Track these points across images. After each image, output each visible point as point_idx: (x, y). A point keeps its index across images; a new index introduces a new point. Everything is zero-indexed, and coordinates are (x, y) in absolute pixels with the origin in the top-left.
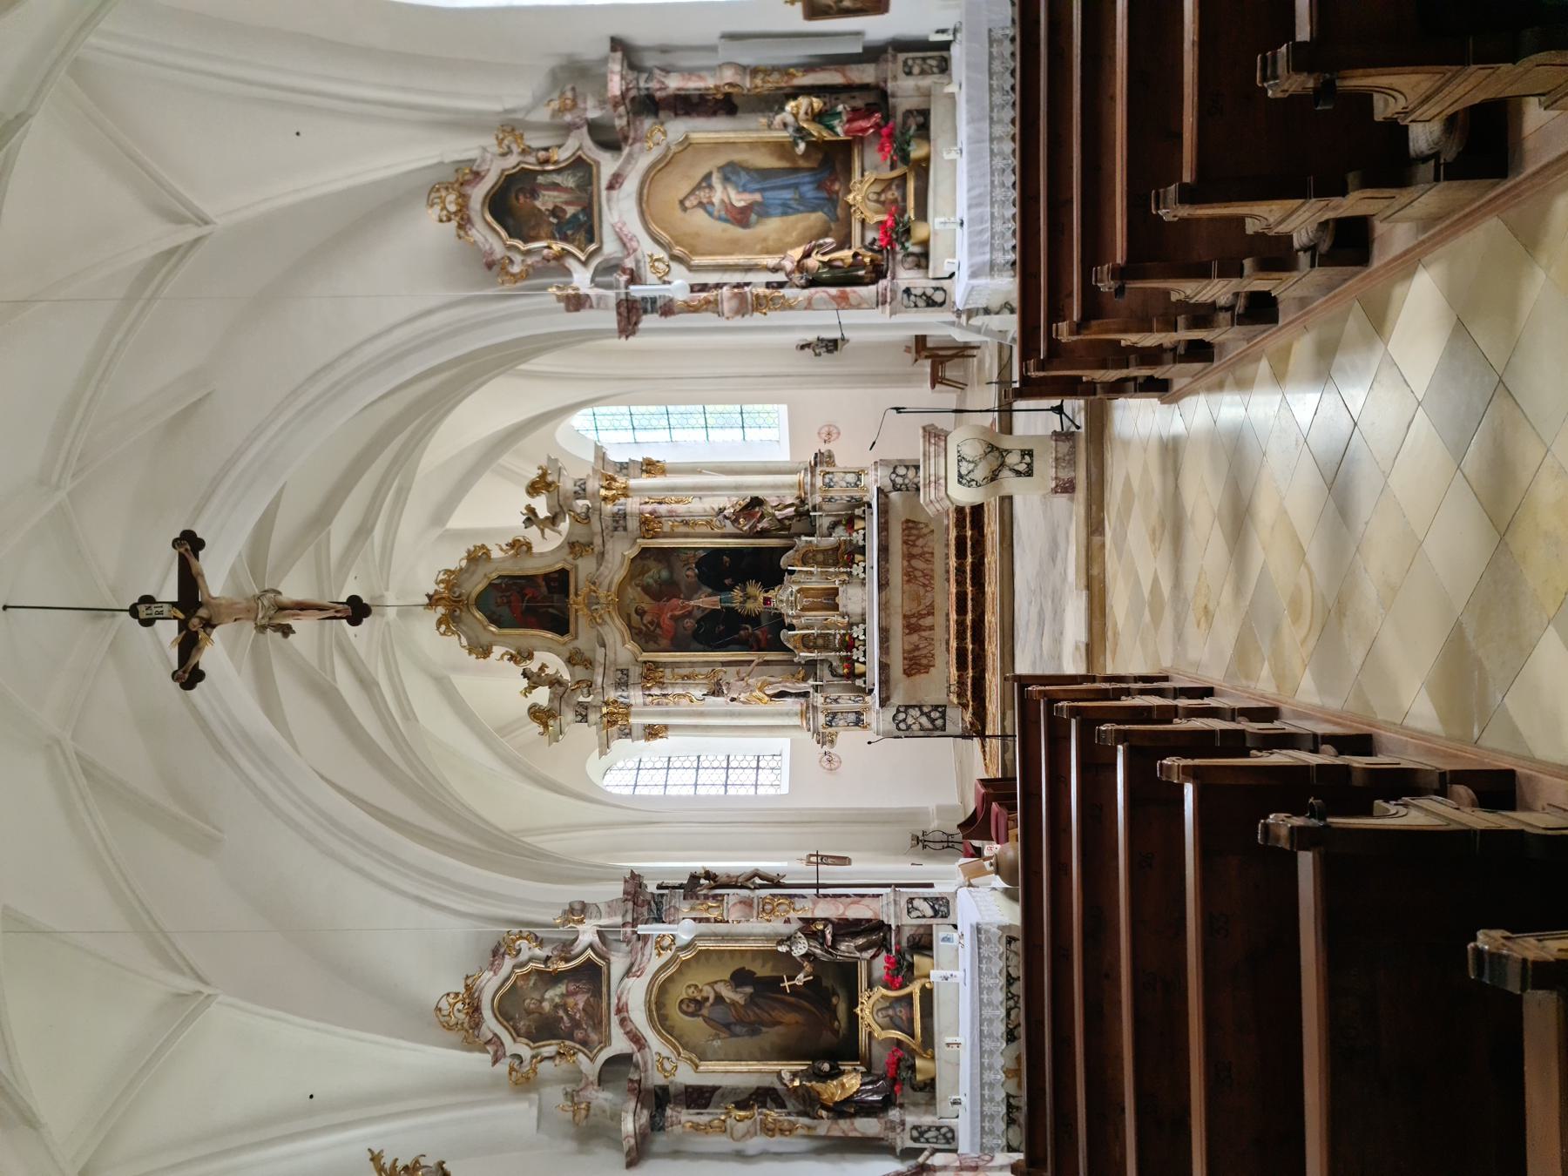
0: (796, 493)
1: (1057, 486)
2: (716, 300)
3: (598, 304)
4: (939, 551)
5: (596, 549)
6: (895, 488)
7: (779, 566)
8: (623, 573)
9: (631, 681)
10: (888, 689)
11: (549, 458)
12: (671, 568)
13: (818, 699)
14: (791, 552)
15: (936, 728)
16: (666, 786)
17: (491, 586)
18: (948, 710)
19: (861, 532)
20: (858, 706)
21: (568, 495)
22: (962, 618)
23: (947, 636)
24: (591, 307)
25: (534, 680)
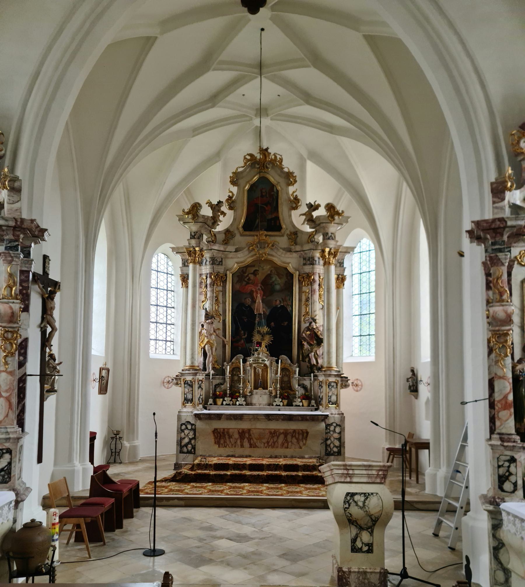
0: (325, 365)
1: (344, 572)
2: (503, 301)
3: (496, 208)
4: (289, 452)
5: (293, 247)
6: (328, 426)
8: (279, 263)
10: (206, 419)
11: (349, 217)
12: (281, 291)
13: (201, 377)
14: (289, 362)
16: (157, 288)
17: (272, 186)
18: (192, 455)
19: (301, 404)
20: (196, 400)
21: (326, 229)
22: (247, 467)
23: (237, 456)
24: (494, 202)
25: (216, 208)
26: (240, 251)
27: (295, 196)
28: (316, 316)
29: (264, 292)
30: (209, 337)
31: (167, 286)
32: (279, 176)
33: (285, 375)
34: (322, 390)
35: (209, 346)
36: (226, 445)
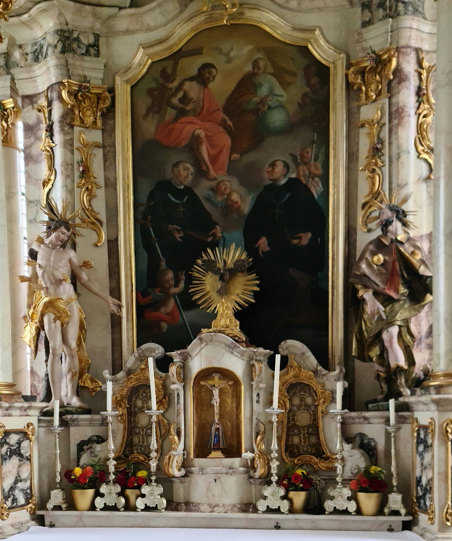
7: (285, 339)
14: (312, 361)
19: (352, 506)
28: (405, 200)
33: (299, 407)
34: (427, 457)
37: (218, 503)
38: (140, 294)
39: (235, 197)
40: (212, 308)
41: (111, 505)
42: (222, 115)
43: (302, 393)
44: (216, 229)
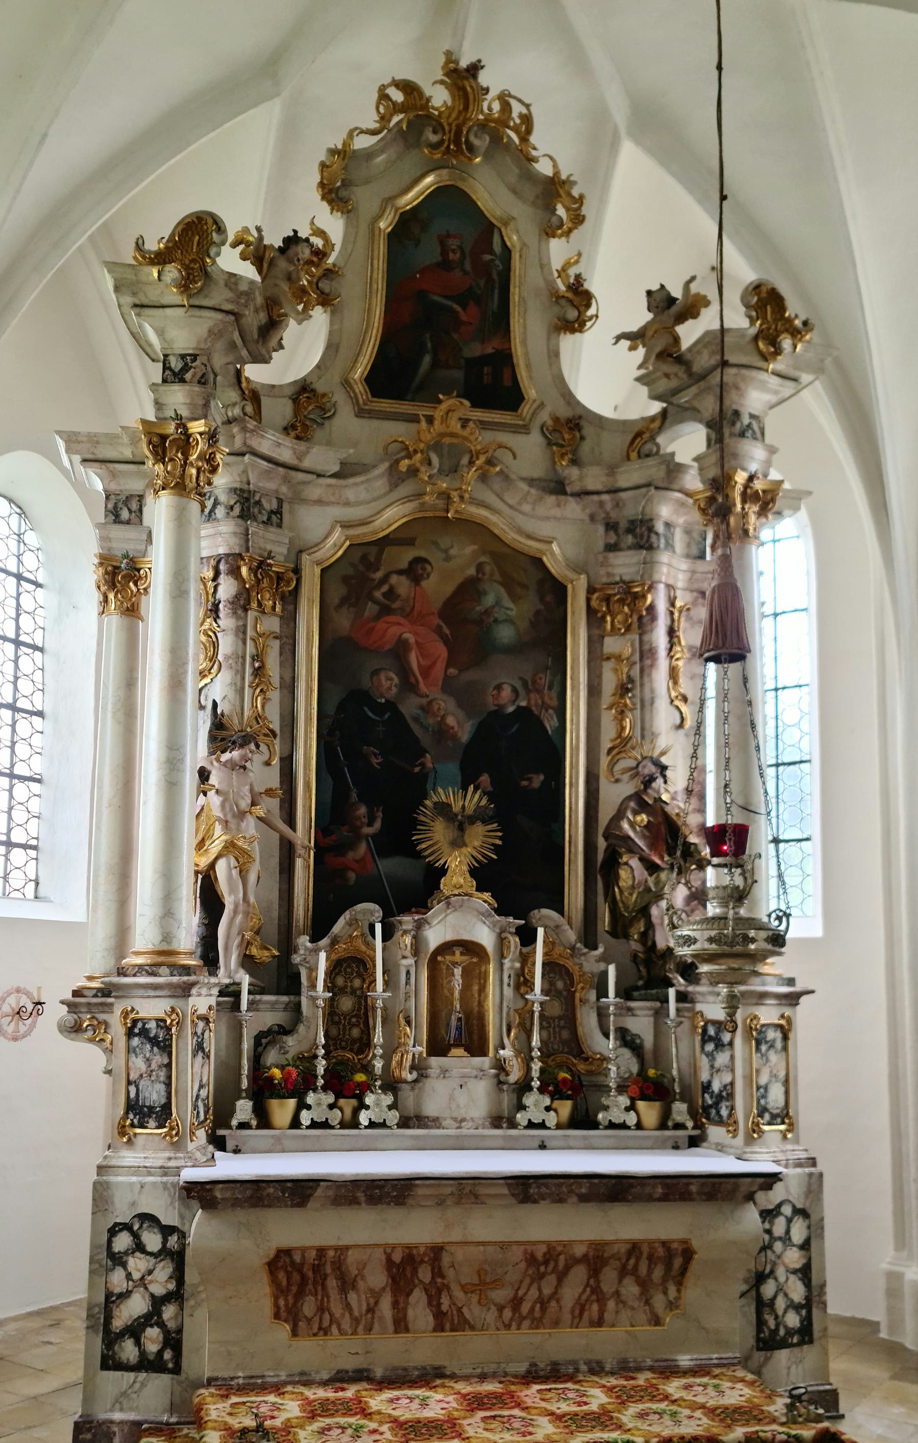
7: (539, 907)
9: (253, 528)
10: (236, 1203)
12: (516, 649)
15: (111, 1339)
18: (166, 1378)
19: (631, 1119)
23: (379, 1373)
26: (353, 474)
27: (572, 280)
29: (449, 654)
30: (233, 825)
31: (18, 628)
32: (515, 192)
35: (233, 862)
36: (326, 1324)
37: (464, 1116)
38: (320, 834)
39: (451, 721)
40: (442, 862)
41: (319, 1121)
42: (437, 621)
43: (551, 975)
44: (425, 757)
